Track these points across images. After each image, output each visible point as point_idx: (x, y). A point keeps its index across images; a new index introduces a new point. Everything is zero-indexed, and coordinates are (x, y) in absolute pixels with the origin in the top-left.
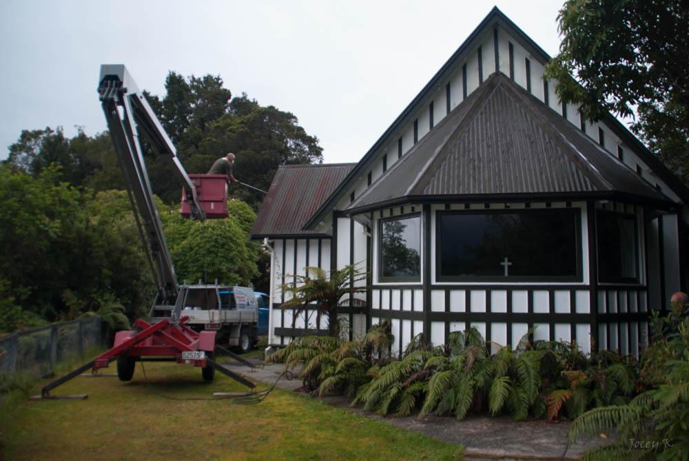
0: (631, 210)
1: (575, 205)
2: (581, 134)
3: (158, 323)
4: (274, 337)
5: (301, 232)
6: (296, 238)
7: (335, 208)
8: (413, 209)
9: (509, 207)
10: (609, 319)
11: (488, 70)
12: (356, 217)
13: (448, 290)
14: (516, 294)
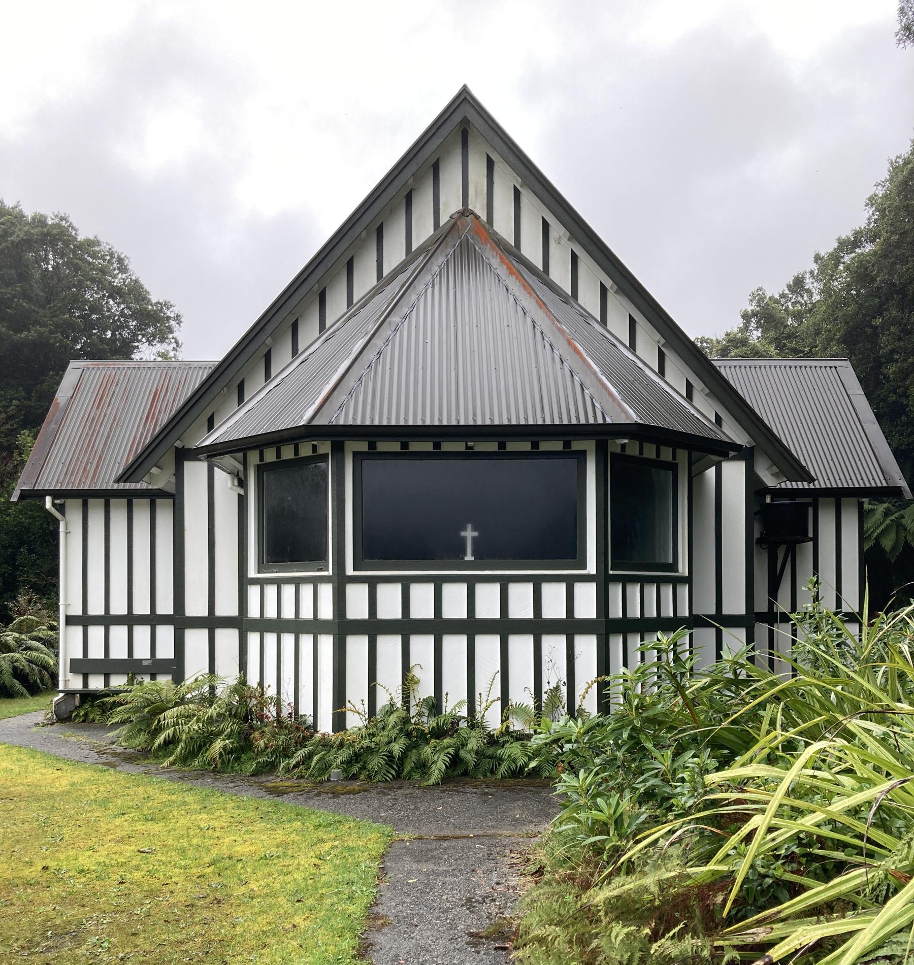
0: (666, 454)
1: (577, 445)
2: (598, 327)
3: (845, 706)
4: (70, 676)
5: (116, 487)
6: (107, 496)
7: (178, 444)
8: (315, 448)
9: (472, 448)
10: (626, 627)
11: (451, 205)
12: (216, 460)
13: (373, 583)
14: (515, 590)
